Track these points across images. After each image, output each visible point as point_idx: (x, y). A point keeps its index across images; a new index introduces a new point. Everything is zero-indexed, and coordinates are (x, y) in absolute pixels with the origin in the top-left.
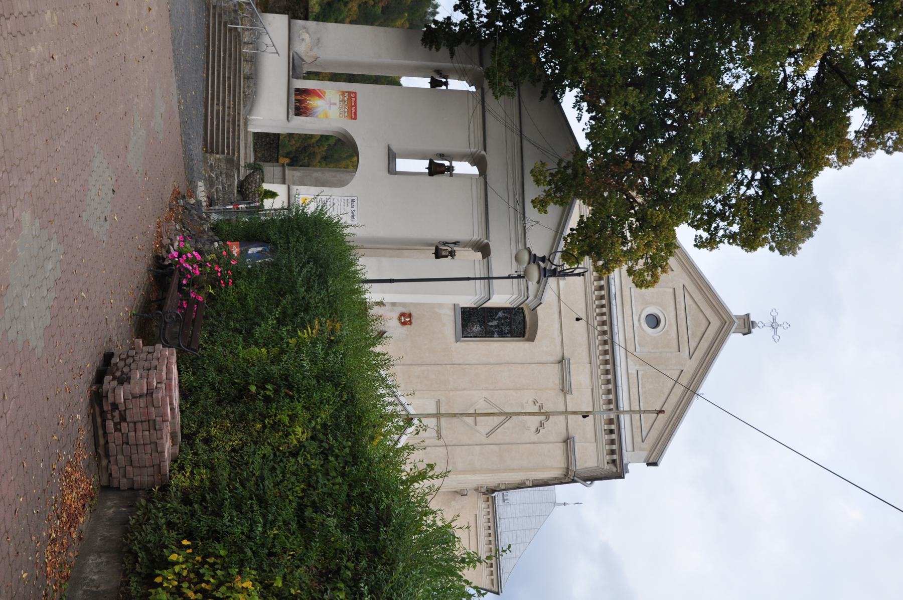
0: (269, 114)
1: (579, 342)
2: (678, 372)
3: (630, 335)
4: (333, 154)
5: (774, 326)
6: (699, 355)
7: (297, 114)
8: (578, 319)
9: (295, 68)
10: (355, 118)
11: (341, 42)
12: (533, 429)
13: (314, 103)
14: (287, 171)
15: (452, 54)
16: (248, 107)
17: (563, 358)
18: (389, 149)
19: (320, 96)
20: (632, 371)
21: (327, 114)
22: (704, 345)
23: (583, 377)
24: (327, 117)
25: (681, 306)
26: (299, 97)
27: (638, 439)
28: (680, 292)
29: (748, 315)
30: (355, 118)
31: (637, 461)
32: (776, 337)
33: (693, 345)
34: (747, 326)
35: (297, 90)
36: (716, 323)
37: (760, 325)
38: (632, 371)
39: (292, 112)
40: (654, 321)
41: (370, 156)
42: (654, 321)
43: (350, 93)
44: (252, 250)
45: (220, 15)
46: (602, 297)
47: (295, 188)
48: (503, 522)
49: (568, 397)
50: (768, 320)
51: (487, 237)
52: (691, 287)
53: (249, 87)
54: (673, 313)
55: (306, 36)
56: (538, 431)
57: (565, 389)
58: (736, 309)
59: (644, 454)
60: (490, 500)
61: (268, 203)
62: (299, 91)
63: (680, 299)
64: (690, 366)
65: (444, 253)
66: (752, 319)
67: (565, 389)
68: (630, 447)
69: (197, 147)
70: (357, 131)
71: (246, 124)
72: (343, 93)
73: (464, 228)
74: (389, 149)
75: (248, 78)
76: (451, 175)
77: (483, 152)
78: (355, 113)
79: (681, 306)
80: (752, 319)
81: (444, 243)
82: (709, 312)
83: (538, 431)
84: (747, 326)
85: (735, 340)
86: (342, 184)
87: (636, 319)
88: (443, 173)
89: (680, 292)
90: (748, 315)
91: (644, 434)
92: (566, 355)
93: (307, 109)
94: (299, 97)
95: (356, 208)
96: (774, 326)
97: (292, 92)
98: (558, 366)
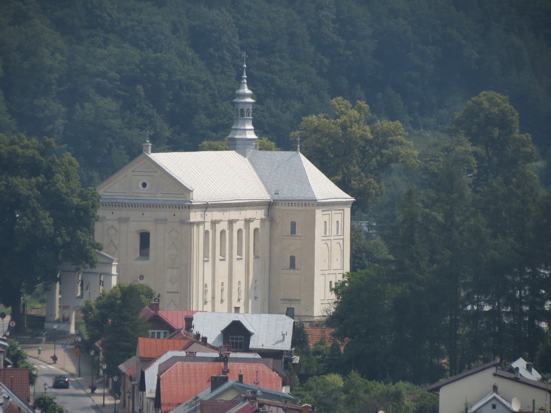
23: (162, 214)
89: (134, 173)
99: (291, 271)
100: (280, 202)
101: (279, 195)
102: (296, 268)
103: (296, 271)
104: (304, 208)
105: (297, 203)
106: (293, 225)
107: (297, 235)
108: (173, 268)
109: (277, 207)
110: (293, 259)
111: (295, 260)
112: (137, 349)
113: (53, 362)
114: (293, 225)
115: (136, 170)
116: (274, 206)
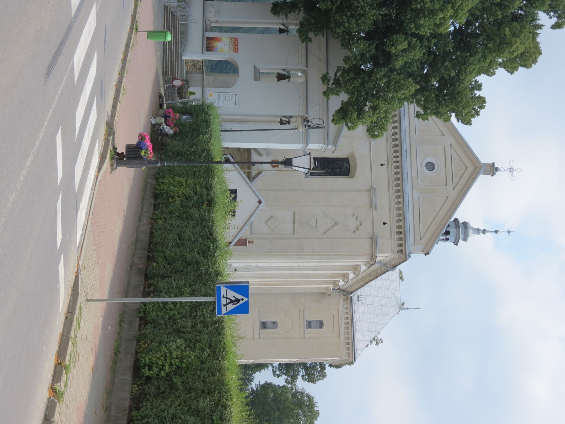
0: (193, 53)
1: (383, 178)
2: (445, 198)
3: (415, 175)
4: (226, 68)
5: (511, 170)
6: (459, 188)
7: (207, 50)
8: (382, 165)
9: (205, 29)
10: (237, 52)
11: (228, 15)
12: (353, 231)
13: (217, 44)
14: (205, 76)
15: (286, 16)
16: (182, 49)
17: (372, 188)
18: (255, 67)
19: (219, 41)
20: (416, 197)
21: (223, 51)
22: (463, 181)
23: (385, 200)
24: (223, 51)
25: (448, 158)
26: (208, 42)
27: (418, 238)
28: (448, 149)
29: (493, 164)
30: (237, 52)
31: (417, 252)
32: (512, 178)
33: (456, 181)
34: (492, 170)
35: (207, 38)
36: (471, 168)
37: (502, 170)
38: (416, 197)
39: (205, 49)
40: (431, 166)
41: (246, 72)
42: (431, 166)
43: (235, 38)
44: (184, 117)
45: (170, 10)
46: (397, 151)
47: (207, 89)
48: (358, 316)
49: (374, 212)
50: (508, 166)
51: (307, 113)
52: (455, 146)
53: (183, 38)
54: (444, 162)
55: (212, 10)
56: (355, 232)
57: (373, 206)
58: (485, 159)
59: (421, 247)
60: (349, 299)
61: (192, 97)
62: (208, 38)
63: (448, 153)
64: (453, 194)
65: (284, 122)
66: (496, 166)
67: (373, 206)
68: (412, 242)
69: (160, 73)
70: (239, 59)
71: (181, 57)
72: (231, 38)
73: (293, 108)
74: (255, 67)
75: (182, 33)
76: (289, 81)
77: (306, 68)
78: (238, 49)
79: (448, 158)
80: (496, 166)
81: (285, 117)
82: (467, 162)
83: (355, 232)
84: (492, 170)
85: (482, 180)
86: (228, 86)
87: (419, 165)
88: (284, 79)
89: (448, 149)
90: (493, 164)
91: (422, 235)
92: (374, 186)
93: (212, 47)
94: (208, 42)
95: (237, 99)
96: (511, 170)
97: (205, 39)
98: (368, 193)
99: (257, 325)
100: (349, 306)
101: (357, 303)
102: (262, 331)
103: (257, 330)
104: (343, 341)
105: (350, 341)
106: (318, 325)
107: (306, 330)
108: (294, 222)
109: (342, 302)
110: (272, 325)
111: (272, 328)
112: (160, 54)
113: (121, 149)
114: (318, 325)
115: (453, 152)
116: (343, 297)
